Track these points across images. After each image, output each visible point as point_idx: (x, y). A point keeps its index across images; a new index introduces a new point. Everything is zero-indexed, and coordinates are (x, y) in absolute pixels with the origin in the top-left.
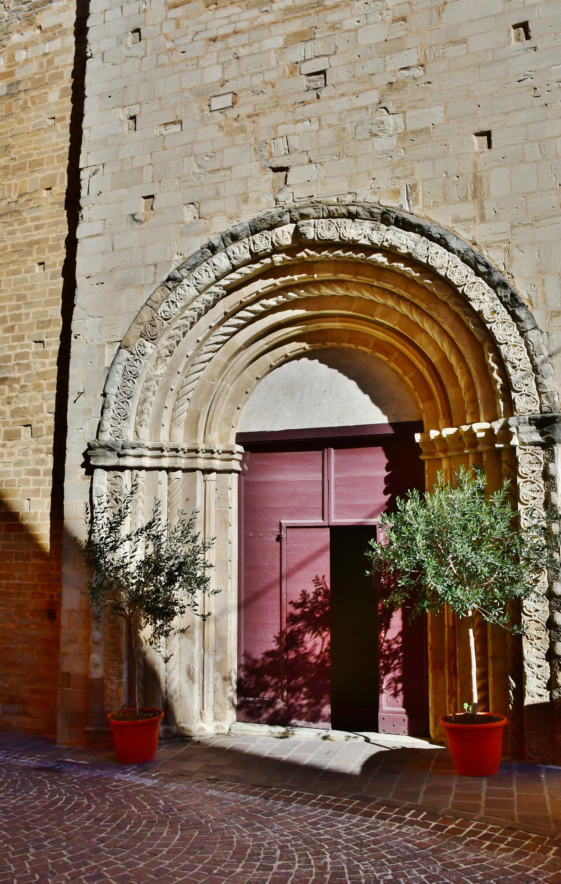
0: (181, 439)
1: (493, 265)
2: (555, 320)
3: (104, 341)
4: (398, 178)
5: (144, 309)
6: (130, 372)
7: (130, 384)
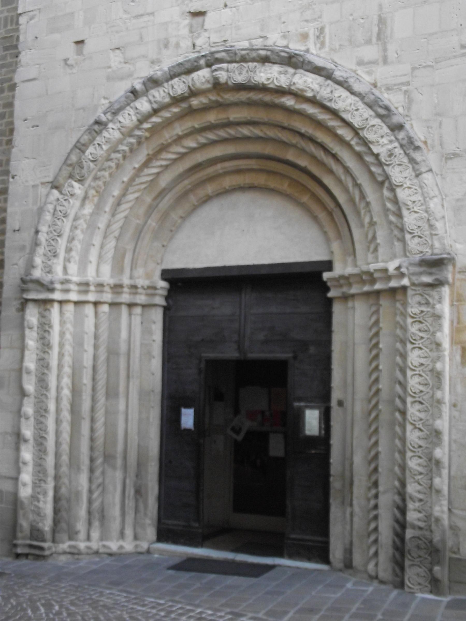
0: (106, 276)
1: (393, 108)
2: (449, 162)
3: (38, 182)
4: (307, 21)
5: (74, 152)
6: (60, 211)
7: (59, 223)
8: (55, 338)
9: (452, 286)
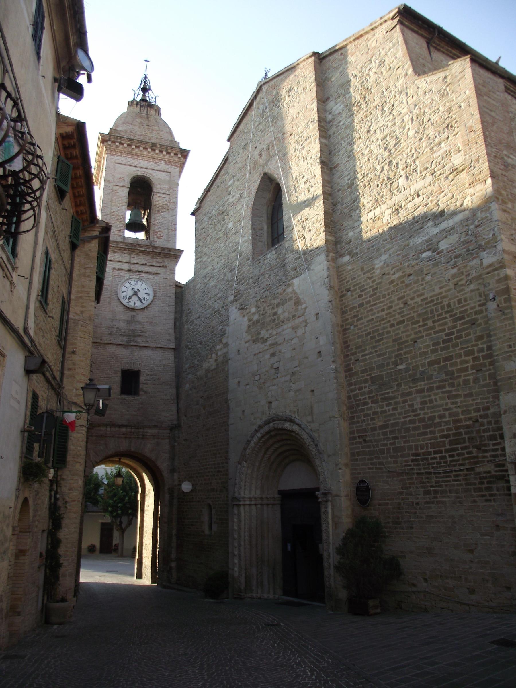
8: (242, 518)
9: (331, 501)
